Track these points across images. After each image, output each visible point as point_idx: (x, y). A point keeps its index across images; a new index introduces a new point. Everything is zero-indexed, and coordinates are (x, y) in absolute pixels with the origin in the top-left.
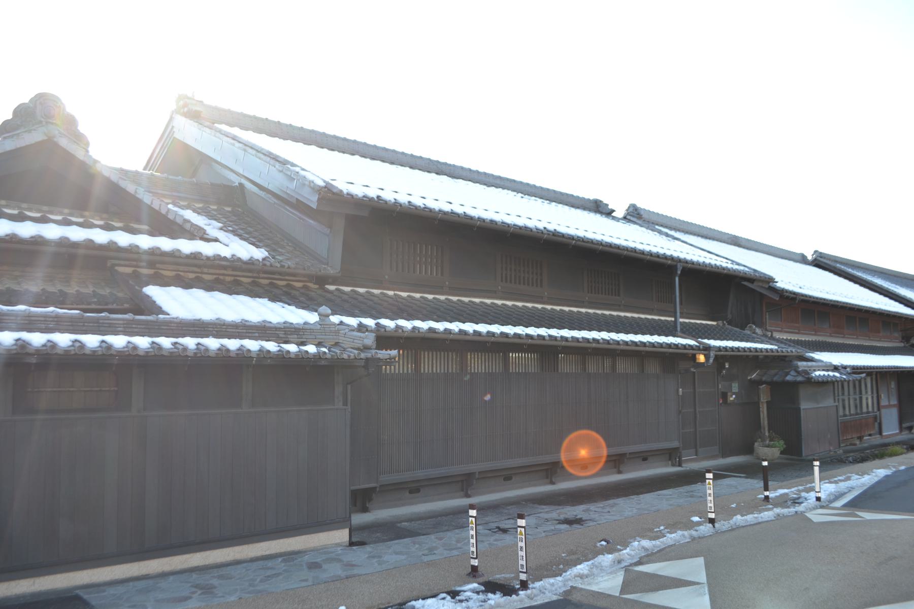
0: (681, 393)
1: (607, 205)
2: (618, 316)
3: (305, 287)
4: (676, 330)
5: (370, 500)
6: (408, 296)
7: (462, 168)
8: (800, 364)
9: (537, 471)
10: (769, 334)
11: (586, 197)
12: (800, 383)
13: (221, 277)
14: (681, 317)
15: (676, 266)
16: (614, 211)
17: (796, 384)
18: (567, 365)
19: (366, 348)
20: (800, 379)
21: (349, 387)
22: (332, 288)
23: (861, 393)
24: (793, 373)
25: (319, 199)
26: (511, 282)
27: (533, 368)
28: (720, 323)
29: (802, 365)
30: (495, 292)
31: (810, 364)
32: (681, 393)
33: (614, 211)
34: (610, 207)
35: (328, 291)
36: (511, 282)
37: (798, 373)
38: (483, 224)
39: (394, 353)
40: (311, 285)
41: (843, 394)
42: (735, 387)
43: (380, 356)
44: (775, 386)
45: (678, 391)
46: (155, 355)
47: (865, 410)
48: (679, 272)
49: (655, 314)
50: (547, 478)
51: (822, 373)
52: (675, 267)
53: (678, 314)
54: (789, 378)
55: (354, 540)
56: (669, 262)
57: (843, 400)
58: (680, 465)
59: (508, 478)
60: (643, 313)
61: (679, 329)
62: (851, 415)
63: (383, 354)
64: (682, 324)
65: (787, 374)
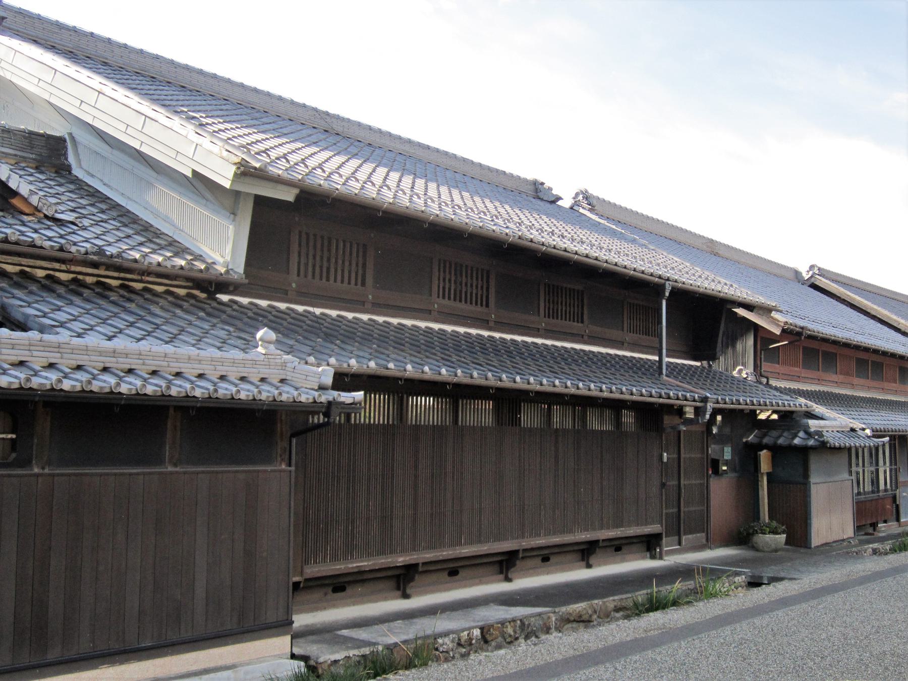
0: (665, 460)
1: (550, 189)
2: (478, 335)
3: (189, 295)
4: (661, 373)
5: (412, 579)
6: (269, 306)
7: (359, 124)
8: (811, 422)
9: (482, 564)
10: (764, 380)
11: (523, 176)
12: (812, 448)
13: (80, 277)
14: (668, 356)
15: (664, 285)
16: (559, 198)
17: (804, 451)
18: (529, 418)
19: (322, 388)
20: (811, 442)
21: (294, 441)
22: (224, 298)
23: (877, 464)
24: (801, 434)
25: (236, 174)
26: (449, 298)
27: (488, 420)
28: (705, 363)
29: (813, 424)
30: (430, 312)
31: (822, 422)
32: (665, 460)
33: (559, 198)
34: (554, 192)
35: (221, 303)
36: (471, 303)
37: (809, 435)
38: (437, 219)
39: (359, 395)
40: (196, 292)
41: (857, 465)
42: (728, 453)
43: (342, 399)
44: (776, 451)
45: (661, 456)
46: (83, 391)
47: (882, 487)
48: (667, 294)
49: (626, 350)
50: (501, 573)
51: (279, 429)
52: (662, 287)
53: (664, 351)
54: (797, 441)
55: (296, 651)
56: (632, 272)
57: (858, 473)
58: (661, 558)
59: (453, 573)
60: (612, 347)
61: (664, 371)
62: (865, 493)
63: (346, 397)
64: (669, 365)
65: (795, 436)
